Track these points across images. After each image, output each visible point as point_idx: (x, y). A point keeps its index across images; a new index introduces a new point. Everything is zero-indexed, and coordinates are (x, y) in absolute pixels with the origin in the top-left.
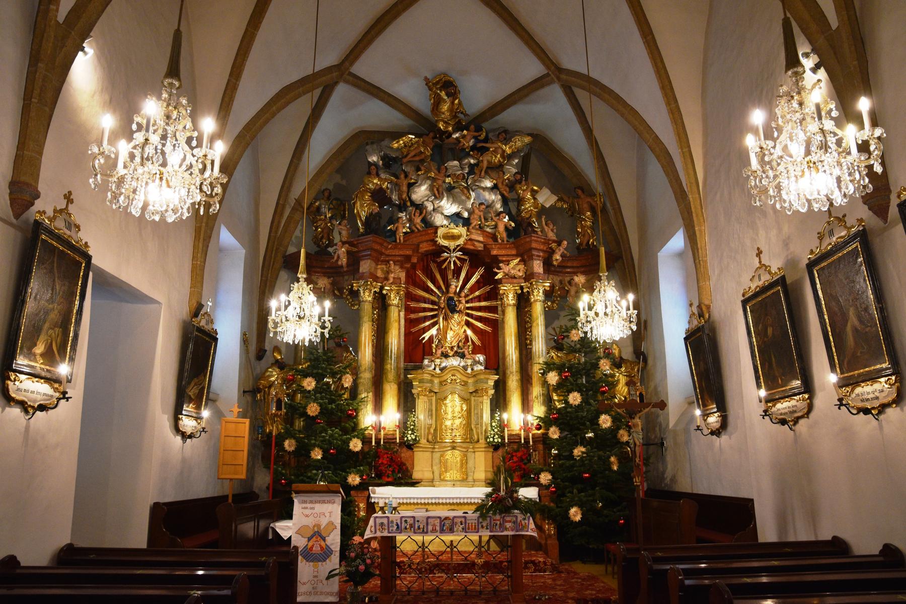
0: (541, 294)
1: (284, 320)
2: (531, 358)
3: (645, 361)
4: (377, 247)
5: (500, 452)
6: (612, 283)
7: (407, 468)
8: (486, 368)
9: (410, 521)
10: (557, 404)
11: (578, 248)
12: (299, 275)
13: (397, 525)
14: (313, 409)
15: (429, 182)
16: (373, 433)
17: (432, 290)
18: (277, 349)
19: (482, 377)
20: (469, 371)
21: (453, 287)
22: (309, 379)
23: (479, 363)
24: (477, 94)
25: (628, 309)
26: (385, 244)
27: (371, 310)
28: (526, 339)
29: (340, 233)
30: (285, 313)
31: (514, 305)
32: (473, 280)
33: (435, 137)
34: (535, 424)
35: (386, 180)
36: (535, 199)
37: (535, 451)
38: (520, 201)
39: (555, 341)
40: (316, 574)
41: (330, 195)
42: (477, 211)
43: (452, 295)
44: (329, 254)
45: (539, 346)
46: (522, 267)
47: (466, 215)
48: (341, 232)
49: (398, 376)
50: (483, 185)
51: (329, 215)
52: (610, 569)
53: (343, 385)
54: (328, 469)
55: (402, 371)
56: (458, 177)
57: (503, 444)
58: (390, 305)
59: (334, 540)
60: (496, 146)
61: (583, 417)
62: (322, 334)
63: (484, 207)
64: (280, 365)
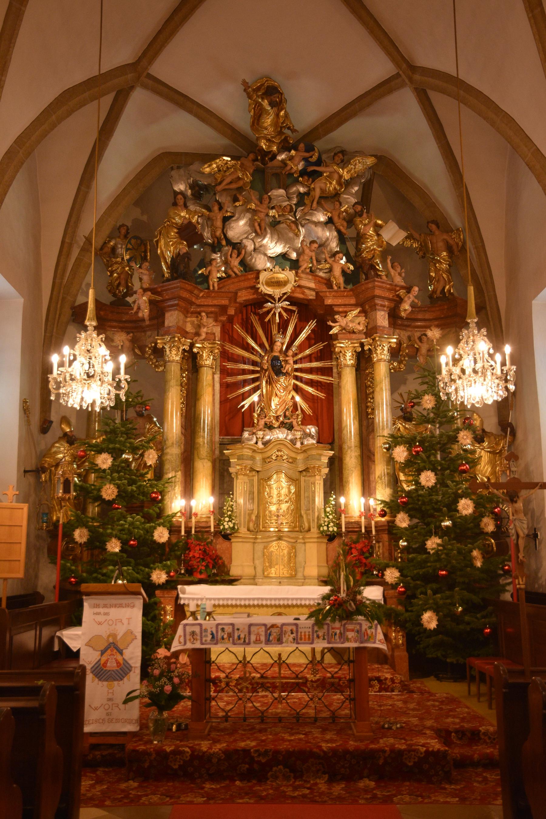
0: (385, 352)
1: (68, 378)
2: (373, 430)
3: (513, 434)
4: (185, 295)
5: (336, 542)
6: (484, 331)
7: (223, 563)
8: (318, 442)
9: (228, 629)
10: (405, 486)
11: (431, 297)
12: (87, 323)
13: (212, 634)
14: (109, 492)
15: (248, 215)
16: (182, 520)
17: (253, 348)
18: (65, 420)
19: (314, 452)
20: (298, 445)
21: (278, 344)
22: (104, 456)
23: (310, 435)
24: (307, 105)
25: (503, 364)
26: (196, 292)
27: (179, 372)
28: (367, 407)
29: (141, 279)
30: (70, 370)
31: (352, 366)
32: (303, 336)
33: (256, 160)
34: (379, 509)
35: (195, 212)
36: (378, 235)
37: (378, 542)
38: (360, 238)
39: (402, 410)
40: (110, 696)
41: (127, 233)
42: (307, 251)
43: (277, 354)
44: (128, 305)
45: (384, 415)
46: (362, 319)
47: (294, 256)
48: (141, 277)
49: (213, 451)
50: (315, 219)
51: (127, 257)
52: (474, 688)
53: (145, 464)
54: (128, 564)
55: (217, 445)
56: (284, 209)
57: (339, 534)
58: (202, 366)
59: (134, 653)
60: (331, 169)
61: (437, 502)
62: (117, 396)
63: (316, 245)
64: (70, 439)
